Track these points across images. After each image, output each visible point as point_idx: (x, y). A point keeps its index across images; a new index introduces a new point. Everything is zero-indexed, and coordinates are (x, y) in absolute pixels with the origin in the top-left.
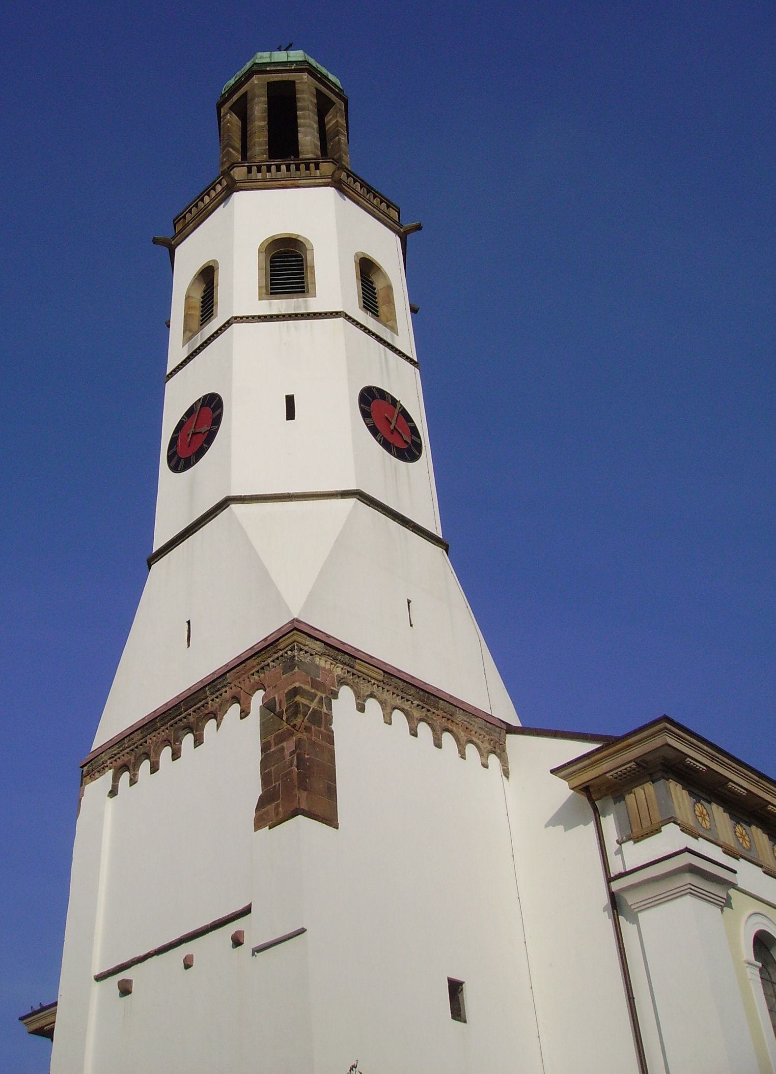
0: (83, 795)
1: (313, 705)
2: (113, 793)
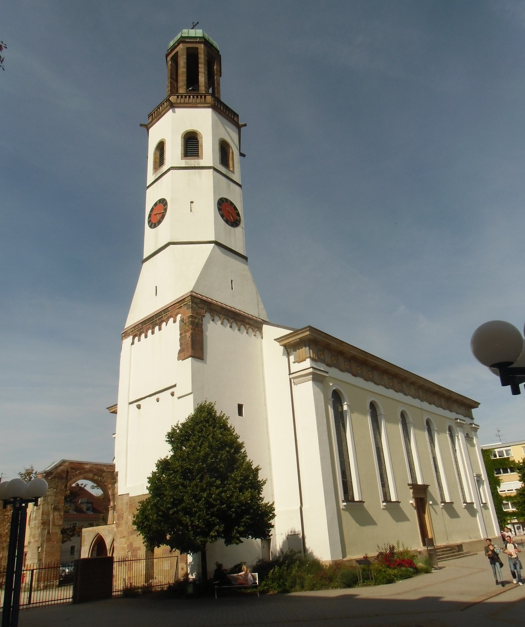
0: (123, 343)
2: (133, 343)
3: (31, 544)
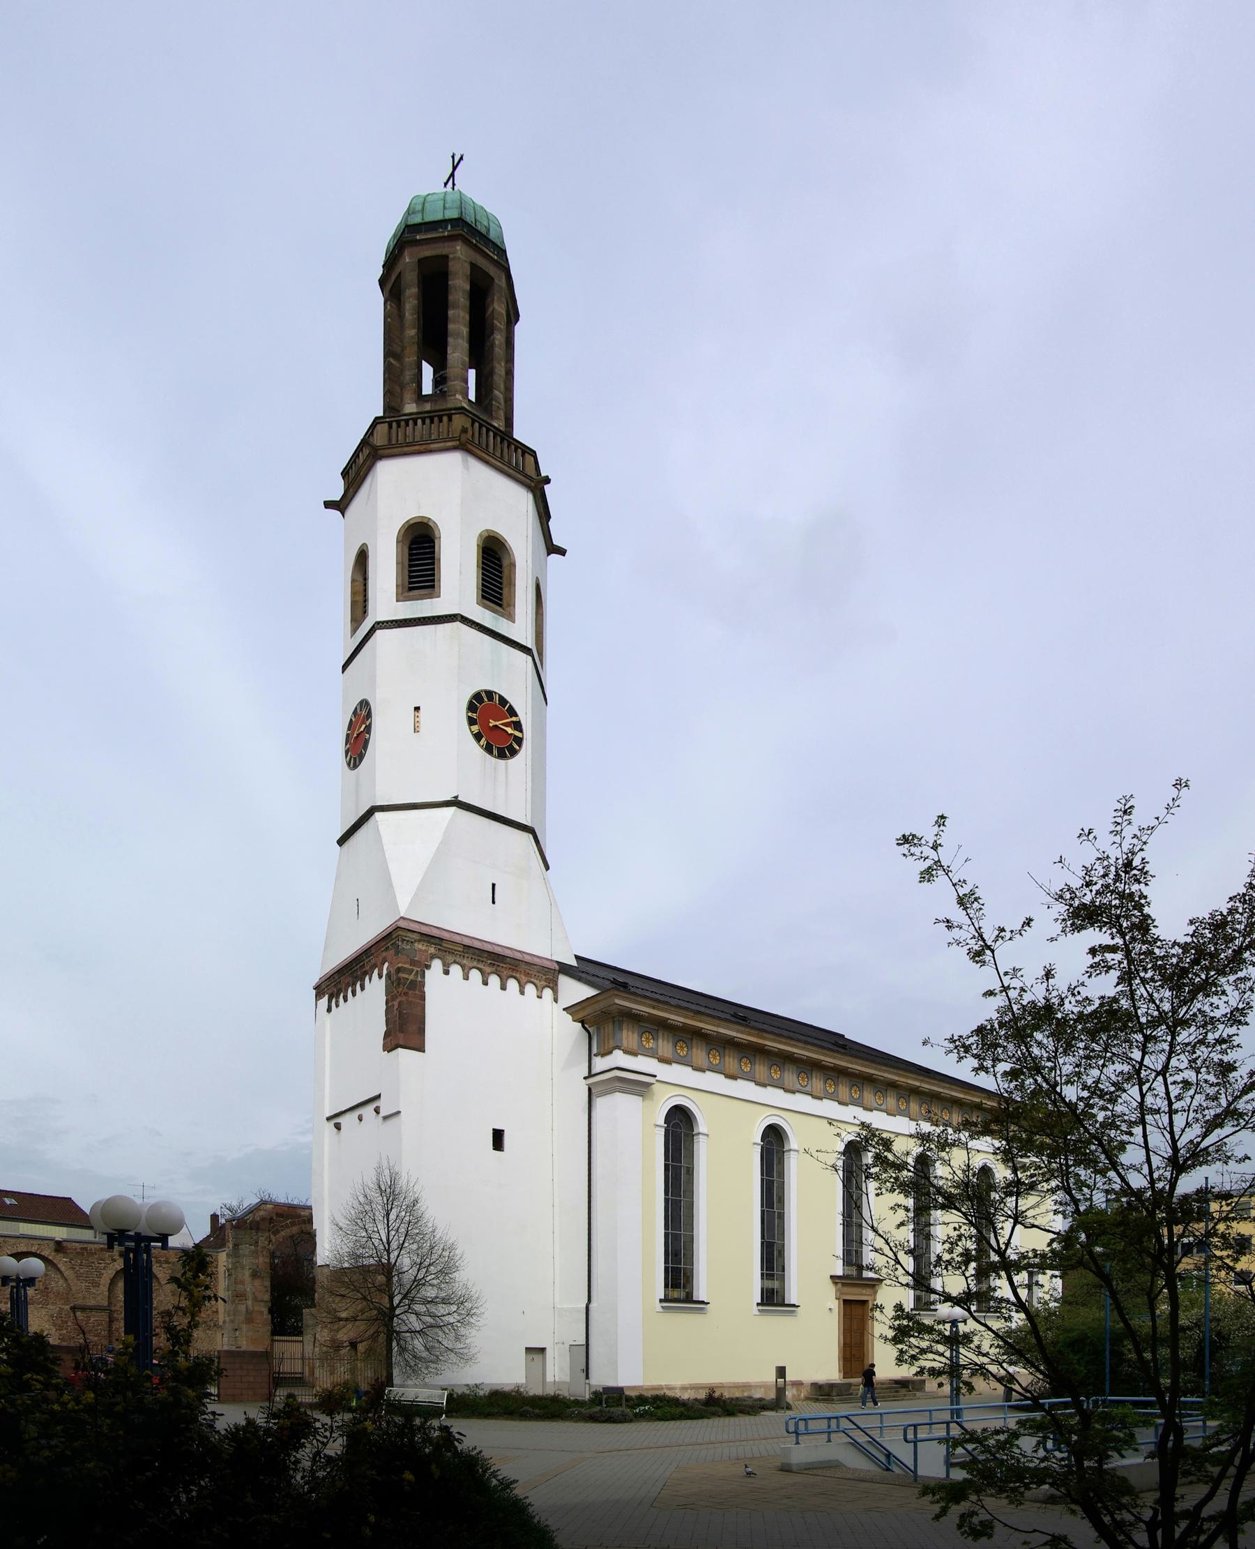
1: (411, 977)
2: (329, 1010)
3: (227, 1325)
